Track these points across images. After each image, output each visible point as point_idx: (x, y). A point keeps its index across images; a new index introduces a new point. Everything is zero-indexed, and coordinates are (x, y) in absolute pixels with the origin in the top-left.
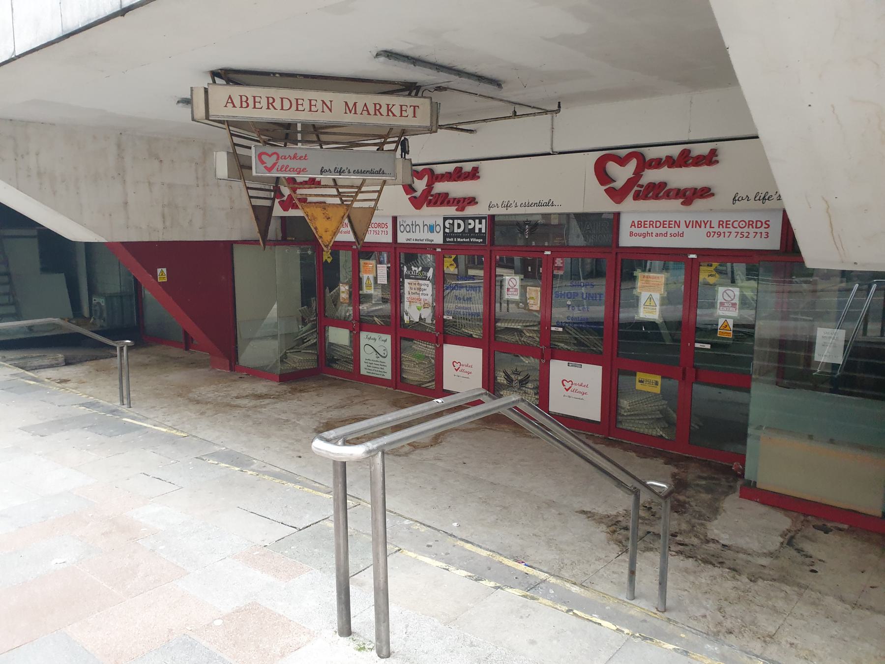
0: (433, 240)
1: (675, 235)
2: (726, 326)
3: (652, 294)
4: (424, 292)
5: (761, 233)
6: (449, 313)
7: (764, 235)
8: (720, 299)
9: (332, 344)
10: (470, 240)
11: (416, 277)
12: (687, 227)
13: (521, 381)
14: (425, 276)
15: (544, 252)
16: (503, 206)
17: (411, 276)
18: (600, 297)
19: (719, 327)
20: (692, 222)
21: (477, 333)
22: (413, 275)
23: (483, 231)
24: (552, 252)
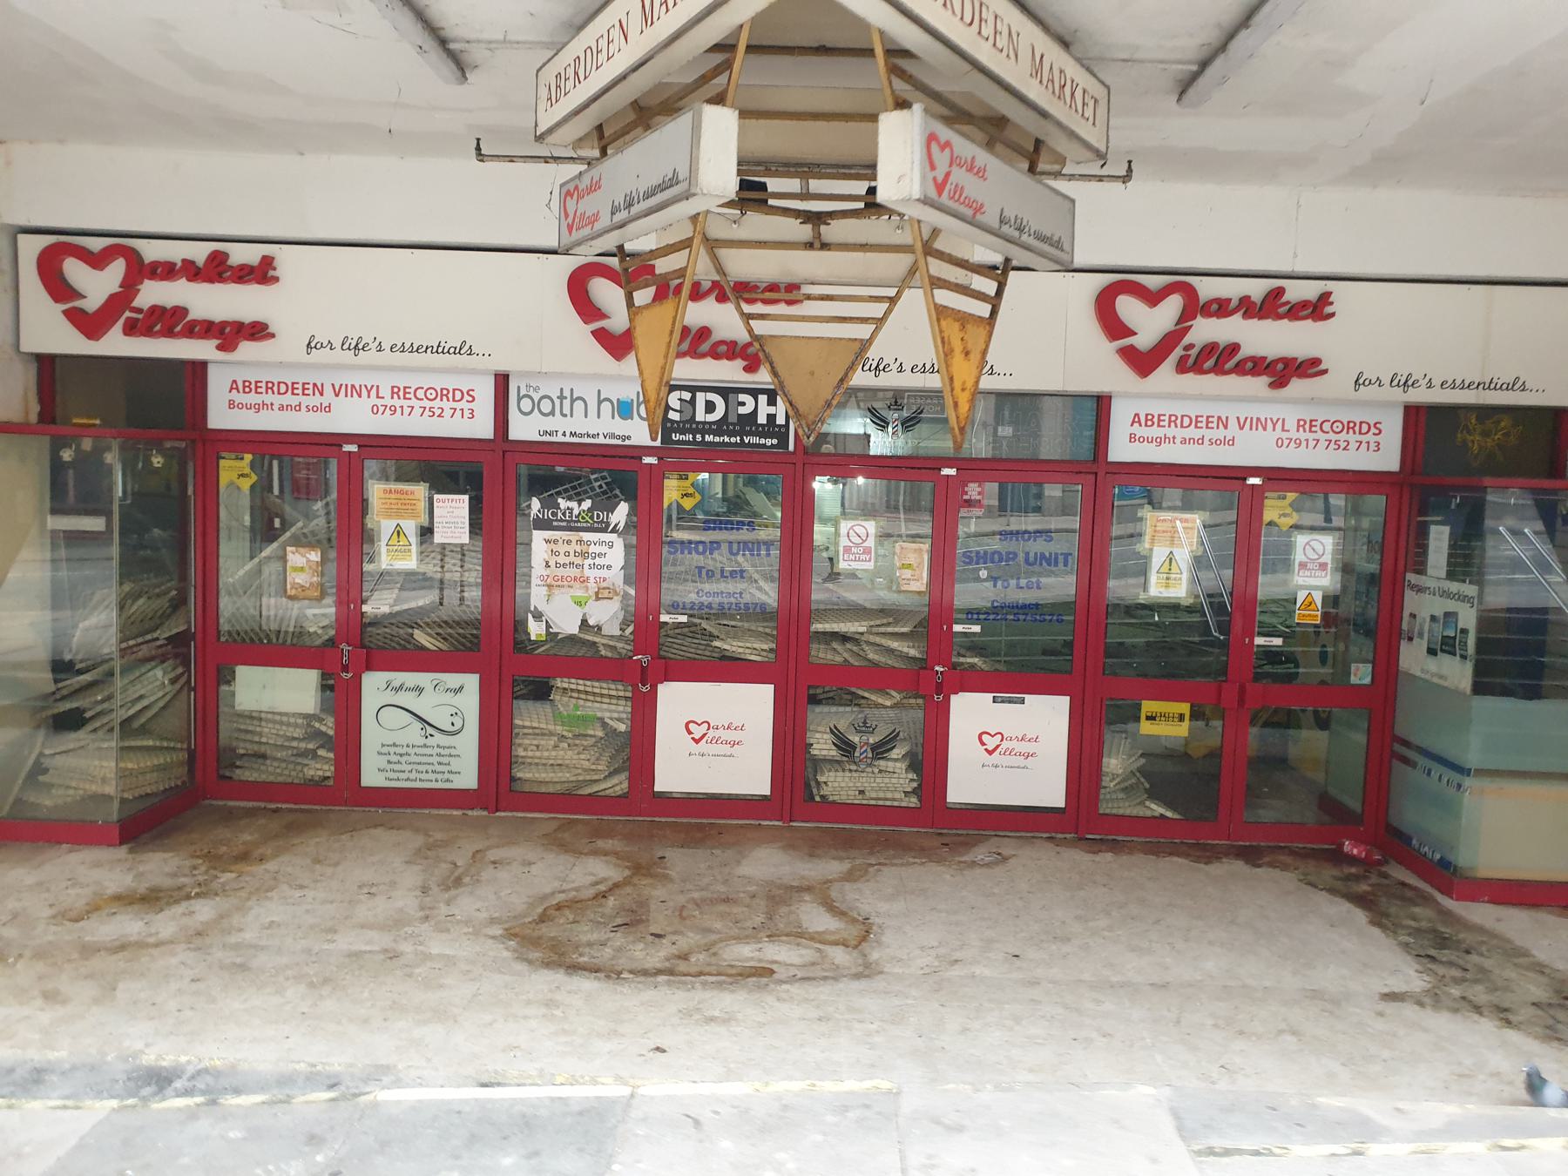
0: (629, 438)
1: (1218, 442)
2: (1311, 604)
3: (402, 523)
4: (597, 561)
5: (1368, 443)
6: (675, 608)
7: (1373, 446)
8: (1299, 556)
9: (250, 716)
10: (742, 440)
11: (572, 524)
12: (337, 395)
13: (874, 748)
14: (602, 521)
15: (1245, 479)
16: (1395, 383)
17: (555, 524)
18: (768, 550)
19: (1298, 606)
20: (1249, 420)
21: (755, 648)
22: (561, 520)
23: (781, 420)
24: (359, 446)
